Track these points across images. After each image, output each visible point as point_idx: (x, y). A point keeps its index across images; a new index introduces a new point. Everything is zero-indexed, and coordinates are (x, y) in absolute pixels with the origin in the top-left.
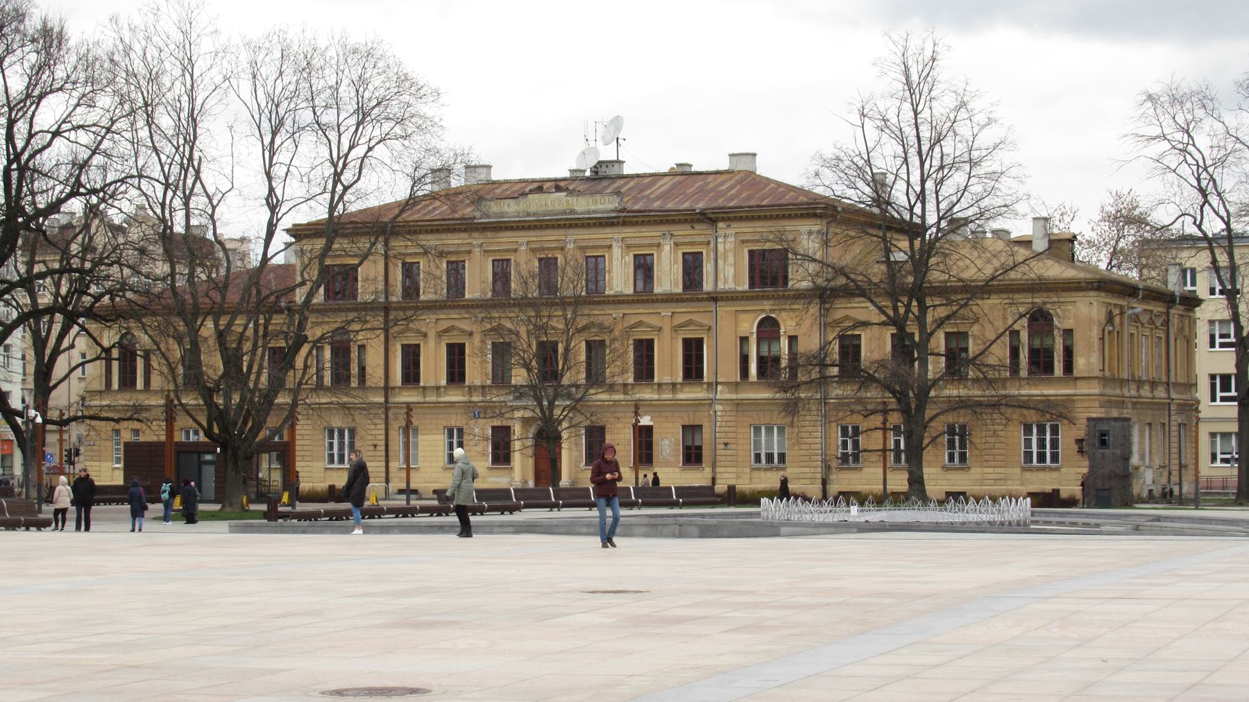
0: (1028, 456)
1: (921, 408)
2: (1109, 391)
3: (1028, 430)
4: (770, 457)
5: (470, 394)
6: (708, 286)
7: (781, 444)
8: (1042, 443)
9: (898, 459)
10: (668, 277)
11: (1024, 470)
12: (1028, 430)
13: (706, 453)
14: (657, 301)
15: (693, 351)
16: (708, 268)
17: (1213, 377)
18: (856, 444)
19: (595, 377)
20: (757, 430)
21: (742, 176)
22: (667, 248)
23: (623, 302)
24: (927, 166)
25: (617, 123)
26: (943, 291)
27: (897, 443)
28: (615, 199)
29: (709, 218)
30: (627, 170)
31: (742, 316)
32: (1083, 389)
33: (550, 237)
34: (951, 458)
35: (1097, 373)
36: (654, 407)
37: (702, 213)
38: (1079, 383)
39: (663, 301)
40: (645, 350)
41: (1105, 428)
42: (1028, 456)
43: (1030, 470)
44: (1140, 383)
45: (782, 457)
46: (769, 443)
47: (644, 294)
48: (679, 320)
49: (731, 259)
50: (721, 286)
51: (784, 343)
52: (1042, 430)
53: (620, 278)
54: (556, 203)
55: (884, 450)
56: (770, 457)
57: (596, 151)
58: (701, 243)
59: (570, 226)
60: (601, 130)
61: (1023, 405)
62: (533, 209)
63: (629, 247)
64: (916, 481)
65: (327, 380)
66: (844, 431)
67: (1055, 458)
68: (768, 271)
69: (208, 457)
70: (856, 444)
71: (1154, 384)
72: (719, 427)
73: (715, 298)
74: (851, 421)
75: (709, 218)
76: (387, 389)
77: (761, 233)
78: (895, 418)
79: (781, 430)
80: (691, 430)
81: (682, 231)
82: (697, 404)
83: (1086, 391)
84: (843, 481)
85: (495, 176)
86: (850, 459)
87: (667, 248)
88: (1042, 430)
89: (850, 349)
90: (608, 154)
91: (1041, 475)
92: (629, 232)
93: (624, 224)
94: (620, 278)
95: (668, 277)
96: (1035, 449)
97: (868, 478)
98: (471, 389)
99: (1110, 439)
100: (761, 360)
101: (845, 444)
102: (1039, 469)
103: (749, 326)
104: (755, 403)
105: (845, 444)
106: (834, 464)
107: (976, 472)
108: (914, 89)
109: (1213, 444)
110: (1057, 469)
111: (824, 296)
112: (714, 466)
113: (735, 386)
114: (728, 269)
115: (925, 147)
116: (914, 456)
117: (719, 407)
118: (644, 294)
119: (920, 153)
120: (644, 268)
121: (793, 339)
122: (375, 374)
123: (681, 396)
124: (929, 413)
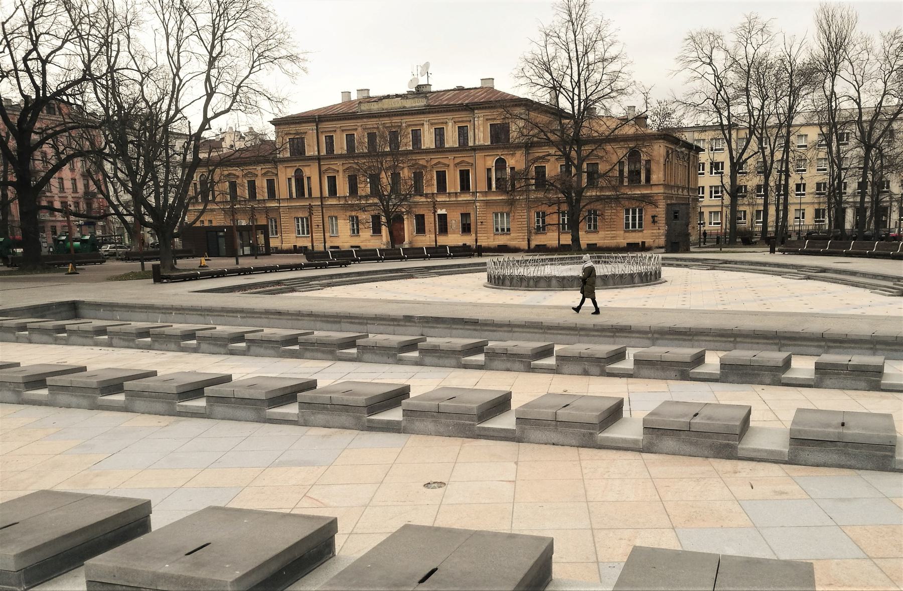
0: (627, 225)
1: (578, 201)
2: (667, 191)
3: (627, 212)
4: (503, 230)
5: (360, 200)
6: (471, 144)
7: (508, 223)
8: (634, 219)
9: (564, 228)
10: (451, 139)
11: (625, 232)
12: (627, 212)
13: (473, 227)
14: (447, 151)
15: (464, 176)
16: (470, 134)
17: (711, 187)
18: (544, 222)
19: (418, 190)
20: (496, 215)
21: (487, 88)
22: (450, 124)
23: (430, 152)
24: (582, 65)
25: (427, 65)
26: (590, 141)
27: (564, 220)
28: (428, 103)
29: (470, 108)
30: (433, 89)
31: (488, 158)
32: (655, 190)
33: (396, 120)
34: (590, 227)
35: (662, 182)
36: (444, 205)
37: (467, 105)
38: (654, 188)
39: (449, 151)
40: (441, 177)
41: (677, 209)
42: (627, 225)
43: (628, 232)
44: (678, 187)
45: (508, 230)
46: (502, 223)
47: (440, 148)
48: (458, 160)
49: (482, 129)
50: (477, 143)
51: (508, 170)
52: (634, 213)
53: (428, 140)
54: (397, 104)
55: (559, 224)
56: (503, 230)
57: (417, 79)
58: (466, 121)
59: (403, 115)
60: (419, 69)
61: (631, 198)
62: (385, 107)
63: (432, 124)
64: (576, 239)
65: (294, 195)
66: (538, 214)
67: (640, 225)
68: (499, 135)
69: (221, 234)
70: (544, 222)
71: (683, 188)
72: (479, 213)
73: (475, 149)
74: (544, 208)
75: (470, 108)
76: (322, 198)
77: (497, 116)
78: (565, 207)
79: (508, 215)
80: (466, 216)
81: (458, 116)
82: (468, 203)
83: (657, 192)
84: (537, 240)
85: (371, 95)
86: (541, 229)
87: (450, 124)
88: (634, 213)
89: (540, 171)
90: (423, 81)
91: (634, 234)
92: (432, 117)
93: (429, 113)
94: (428, 140)
95: (451, 139)
96: (630, 222)
97: (551, 239)
98: (361, 197)
99: (680, 215)
100: (497, 180)
101: (538, 221)
102: (632, 231)
103: (491, 162)
104: (495, 202)
105: (538, 221)
106: (533, 231)
107: (602, 234)
108: (574, 22)
109: (710, 216)
110: (641, 231)
111: (528, 146)
112: (476, 234)
113: (485, 193)
114: (481, 135)
115: (580, 58)
116: (574, 226)
117: (478, 204)
118: (440, 148)
119: (577, 59)
120: (440, 134)
121: (512, 169)
122: (316, 193)
123: (460, 199)
124: (582, 204)
